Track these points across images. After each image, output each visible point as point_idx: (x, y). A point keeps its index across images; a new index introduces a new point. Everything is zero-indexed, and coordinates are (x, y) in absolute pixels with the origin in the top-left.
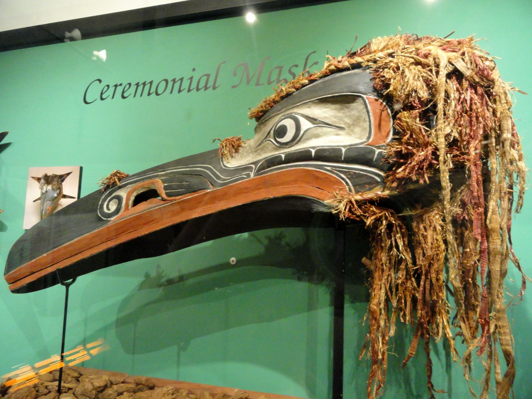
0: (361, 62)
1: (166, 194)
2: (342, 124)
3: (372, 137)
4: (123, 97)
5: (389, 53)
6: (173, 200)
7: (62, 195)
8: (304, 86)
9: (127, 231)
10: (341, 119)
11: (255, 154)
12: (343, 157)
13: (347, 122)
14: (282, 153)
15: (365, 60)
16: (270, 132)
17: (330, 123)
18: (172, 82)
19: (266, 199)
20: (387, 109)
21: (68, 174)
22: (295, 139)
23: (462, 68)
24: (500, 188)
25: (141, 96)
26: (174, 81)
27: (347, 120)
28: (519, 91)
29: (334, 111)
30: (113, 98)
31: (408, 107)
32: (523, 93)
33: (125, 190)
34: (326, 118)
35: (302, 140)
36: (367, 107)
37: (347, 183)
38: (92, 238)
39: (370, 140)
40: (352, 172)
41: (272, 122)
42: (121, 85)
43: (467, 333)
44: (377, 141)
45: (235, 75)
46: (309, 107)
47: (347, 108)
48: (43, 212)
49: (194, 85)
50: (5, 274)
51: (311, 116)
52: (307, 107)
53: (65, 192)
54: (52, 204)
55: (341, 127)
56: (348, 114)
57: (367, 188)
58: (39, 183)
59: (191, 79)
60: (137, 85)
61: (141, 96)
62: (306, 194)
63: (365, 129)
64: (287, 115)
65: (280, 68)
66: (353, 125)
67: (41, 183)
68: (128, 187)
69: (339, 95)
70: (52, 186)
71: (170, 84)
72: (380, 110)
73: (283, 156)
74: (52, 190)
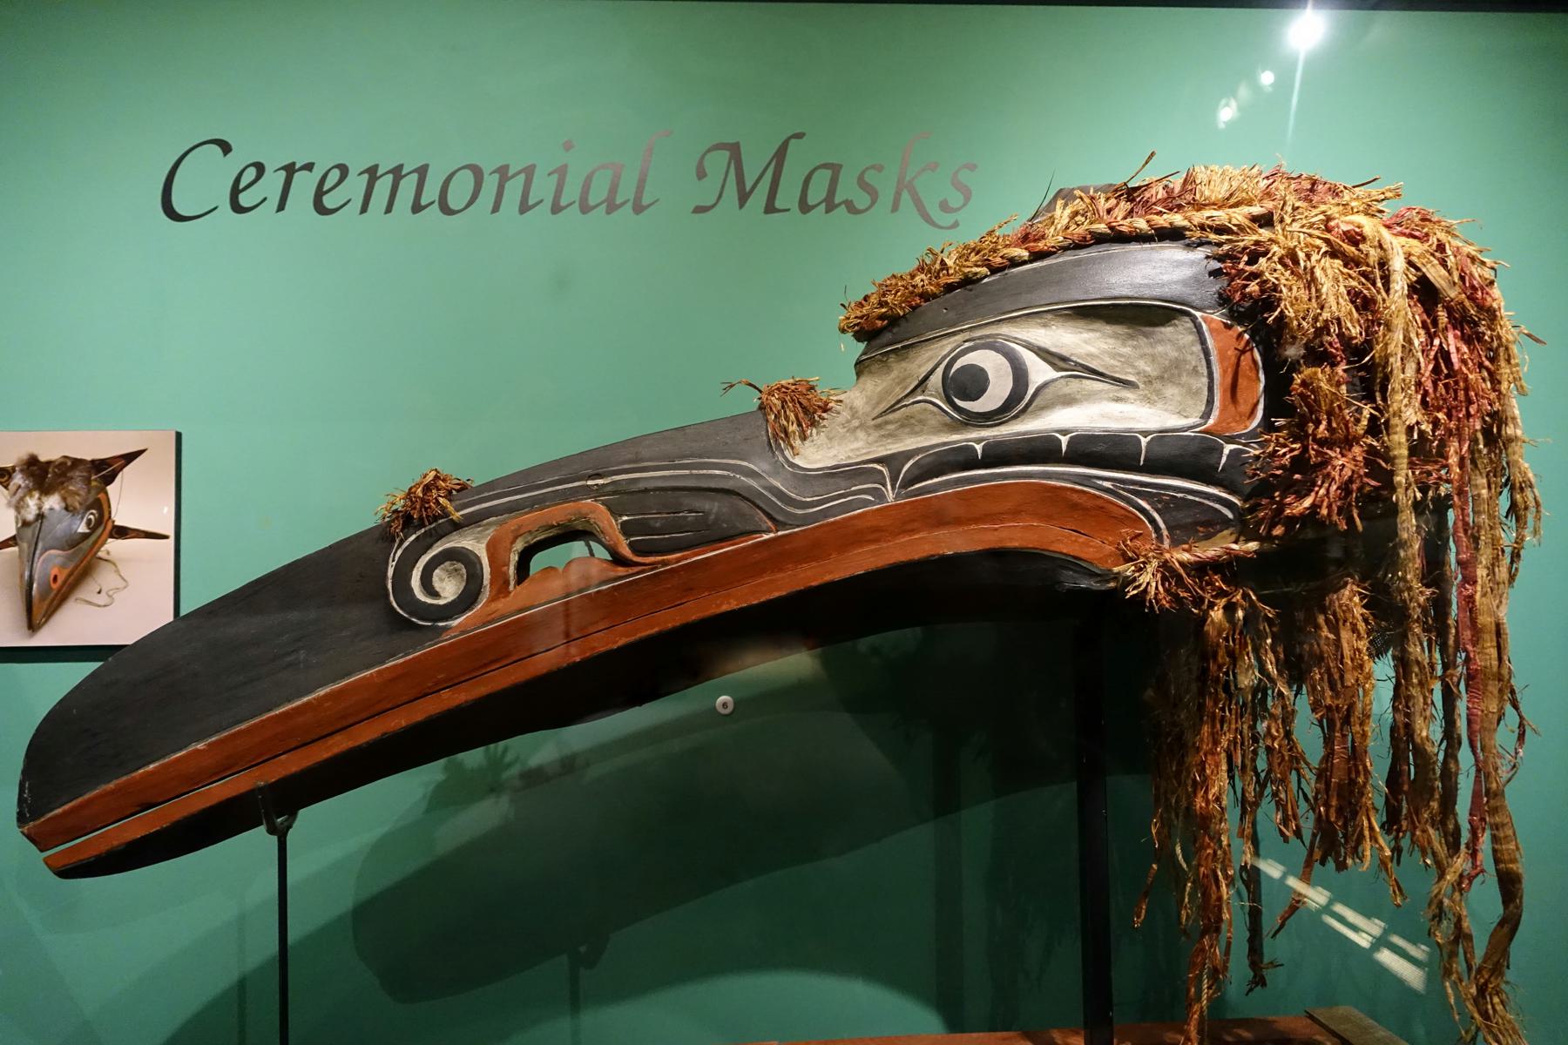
0: (1185, 228)
1: (631, 545)
2: (1130, 373)
3: (1215, 413)
4: (321, 209)
5: (1254, 214)
6: (658, 562)
7: (109, 527)
8: (1014, 262)
9: (507, 656)
10: (1128, 362)
11: (876, 434)
12: (1142, 459)
13: (1144, 371)
14: (977, 439)
15: (1196, 223)
16: (926, 378)
17: (1101, 370)
18: (497, 176)
19: (933, 558)
20: (1252, 350)
21: (130, 457)
22: (1014, 405)
23: (1439, 280)
24: (1493, 540)
25: (389, 210)
26: (503, 173)
27: (1144, 366)
28: (1529, 335)
29: (1111, 341)
30: (281, 207)
31: (1317, 356)
32: (1537, 340)
33: (479, 533)
34: (1090, 355)
35: (1030, 409)
36: (1203, 342)
37: (1153, 521)
38: (393, 680)
39: (1211, 422)
40: (1168, 495)
41: (930, 353)
42: (309, 167)
43: (1441, 847)
44: (1228, 423)
45: (701, 174)
46: (1045, 326)
47: (1146, 336)
48: (35, 586)
49: (571, 193)
50: (22, 819)
51: (1053, 350)
52: (1039, 324)
53: (120, 518)
54: (69, 558)
55: (1127, 380)
56: (1148, 350)
57: (1201, 534)
58: (6, 487)
59: (562, 172)
60: (372, 173)
61: (389, 210)
62: (1045, 547)
63: (1197, 392)
64: (979, 338)
65: (835, 169)
66: (1161, 378)
67: (12, 486)
68: (490, 524)
69: (1131, 304)
70: (64, 499)
71: (490, 184)
72: (1236, 349)
73: (979, 448)
74: (64, 512)
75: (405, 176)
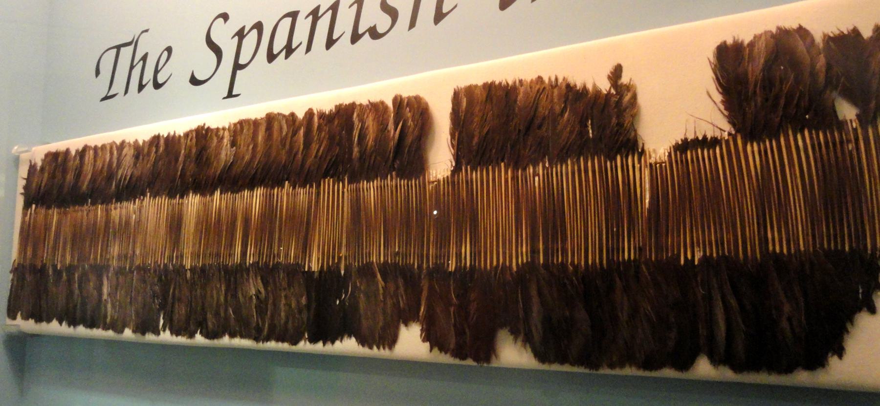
75: (135, 66)
